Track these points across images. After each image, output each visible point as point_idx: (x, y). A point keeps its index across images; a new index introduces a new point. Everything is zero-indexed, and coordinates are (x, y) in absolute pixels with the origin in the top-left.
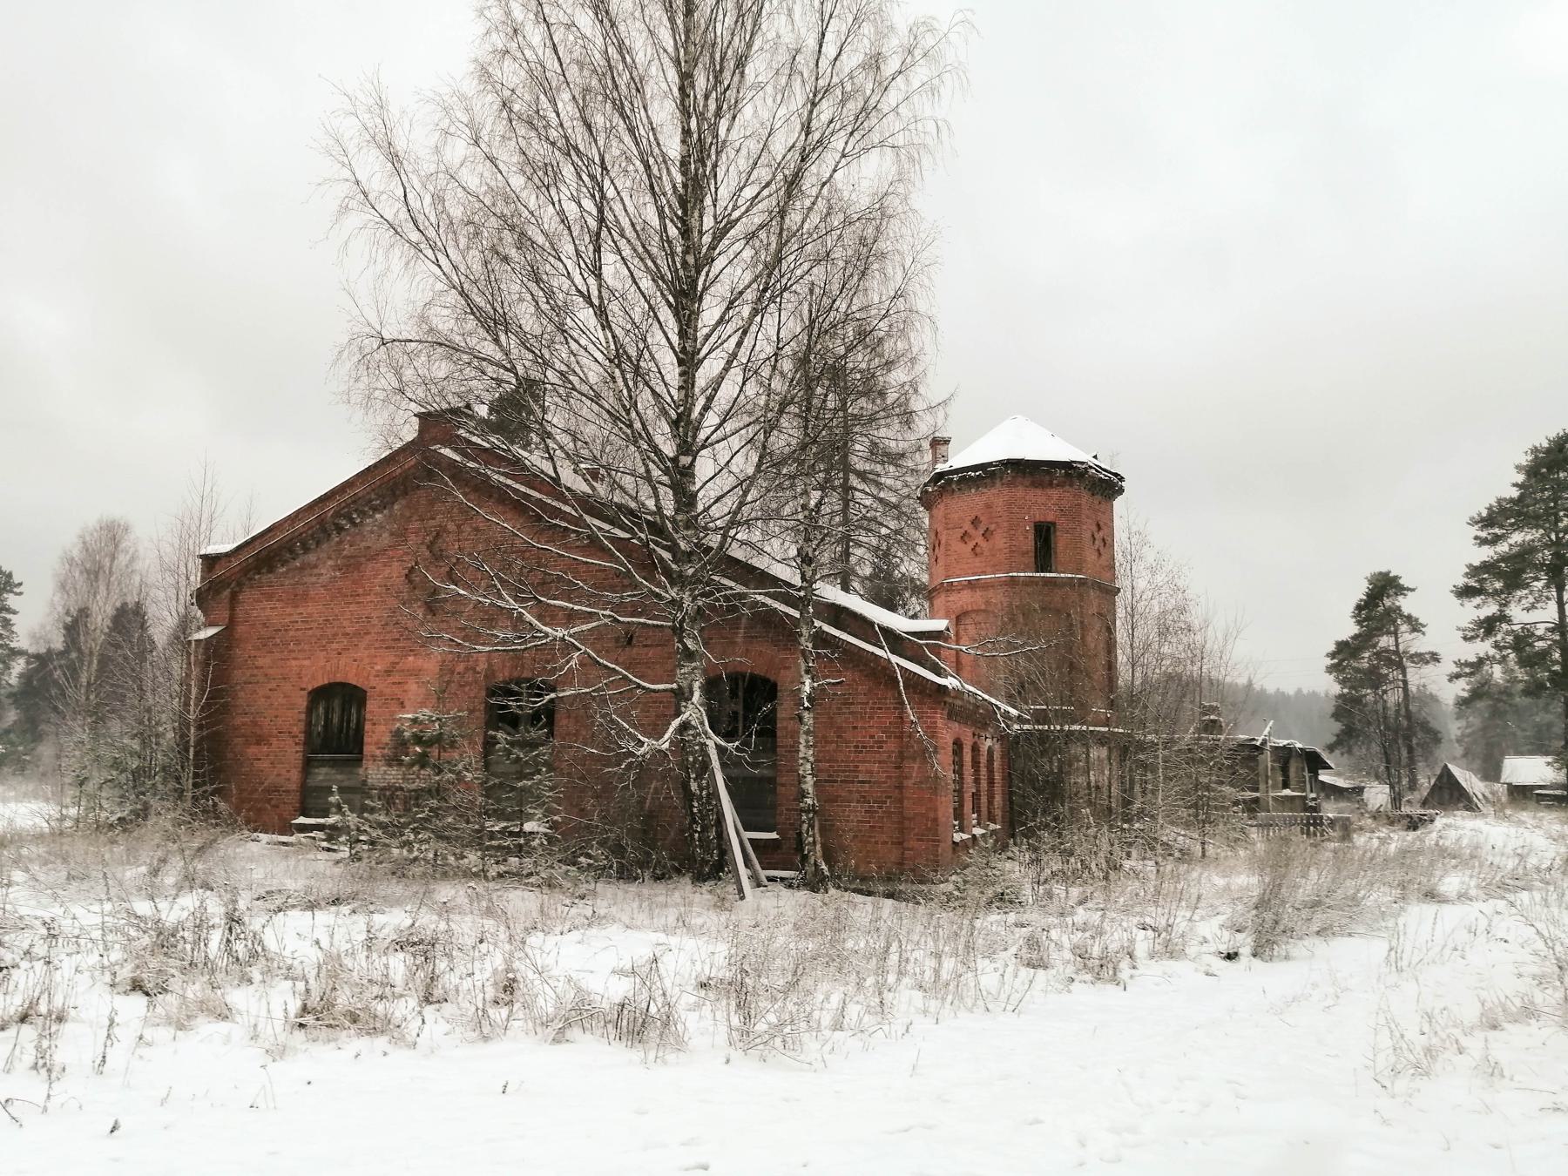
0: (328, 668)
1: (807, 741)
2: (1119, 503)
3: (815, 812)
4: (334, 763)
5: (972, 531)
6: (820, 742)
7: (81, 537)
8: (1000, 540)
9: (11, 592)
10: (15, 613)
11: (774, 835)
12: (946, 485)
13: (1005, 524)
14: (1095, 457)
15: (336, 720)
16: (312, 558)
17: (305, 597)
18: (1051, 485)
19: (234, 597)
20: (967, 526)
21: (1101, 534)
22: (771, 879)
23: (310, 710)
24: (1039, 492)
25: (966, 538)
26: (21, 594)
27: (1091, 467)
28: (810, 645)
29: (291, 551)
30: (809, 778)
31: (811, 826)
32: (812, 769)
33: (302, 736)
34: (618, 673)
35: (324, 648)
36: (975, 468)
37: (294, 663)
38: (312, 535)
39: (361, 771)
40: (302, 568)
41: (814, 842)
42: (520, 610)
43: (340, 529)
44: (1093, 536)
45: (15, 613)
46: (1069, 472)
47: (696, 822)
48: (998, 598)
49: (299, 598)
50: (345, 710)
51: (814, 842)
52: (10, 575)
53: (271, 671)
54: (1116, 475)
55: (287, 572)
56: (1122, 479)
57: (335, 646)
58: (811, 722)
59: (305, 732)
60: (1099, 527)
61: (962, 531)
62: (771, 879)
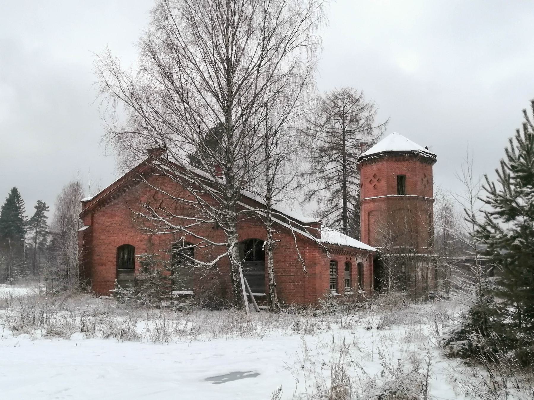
0: (123, 239)
1: (271, 262)
2: (435, 166)
3: (275, 286)
4: (126, 272)
5: (373, 179)
6: (276, 262)
7: (64, 190)
8: (383, 183)
9: (45, 210)
10: (47, 218)
11: (264, 294)
12: (364, 162)
13: (386, 176)
14: (426, 148)
15: (126, 256)
16: (116, 201)
17: (115, 216)
18: (404, 160)
19: (93, 216)
20: (372, 178)
21: (426, 178)
22: (261, 309)
23: (118, 254)
24: (399, 163)
25: (371, 182)
26: (48, 211)
27: (420, 153)
28: (270, 229)
29: (110, 199)
30: (272, 274)
31: (273, 291)
32: (273, 271)
33: (115, 263)
34: (204, 240)
35: (121, 233)
36: (373, 155)
37: (112, 238)
38: (116, 194)
39: (134, 274)
40: (114, 205)
41: (274, 296)
42: (164, 220)
43: (124, 191)
44: (422, 179)
45: (47, 218)
46: (412, 155)
47: (236, 290)
48: (384, 206)
49: (112, 216)
50: (129, 254)
51: (274, 296)
52: (45, 204)
53: (105, 241)
54: (433, 155)
55: (109, 206)
56: (436, 156)
57: (124, 231)
58: (272, 255)
59: (117, 261)
60: (425, 176)
61: (370, 179)
62: (261, 309)
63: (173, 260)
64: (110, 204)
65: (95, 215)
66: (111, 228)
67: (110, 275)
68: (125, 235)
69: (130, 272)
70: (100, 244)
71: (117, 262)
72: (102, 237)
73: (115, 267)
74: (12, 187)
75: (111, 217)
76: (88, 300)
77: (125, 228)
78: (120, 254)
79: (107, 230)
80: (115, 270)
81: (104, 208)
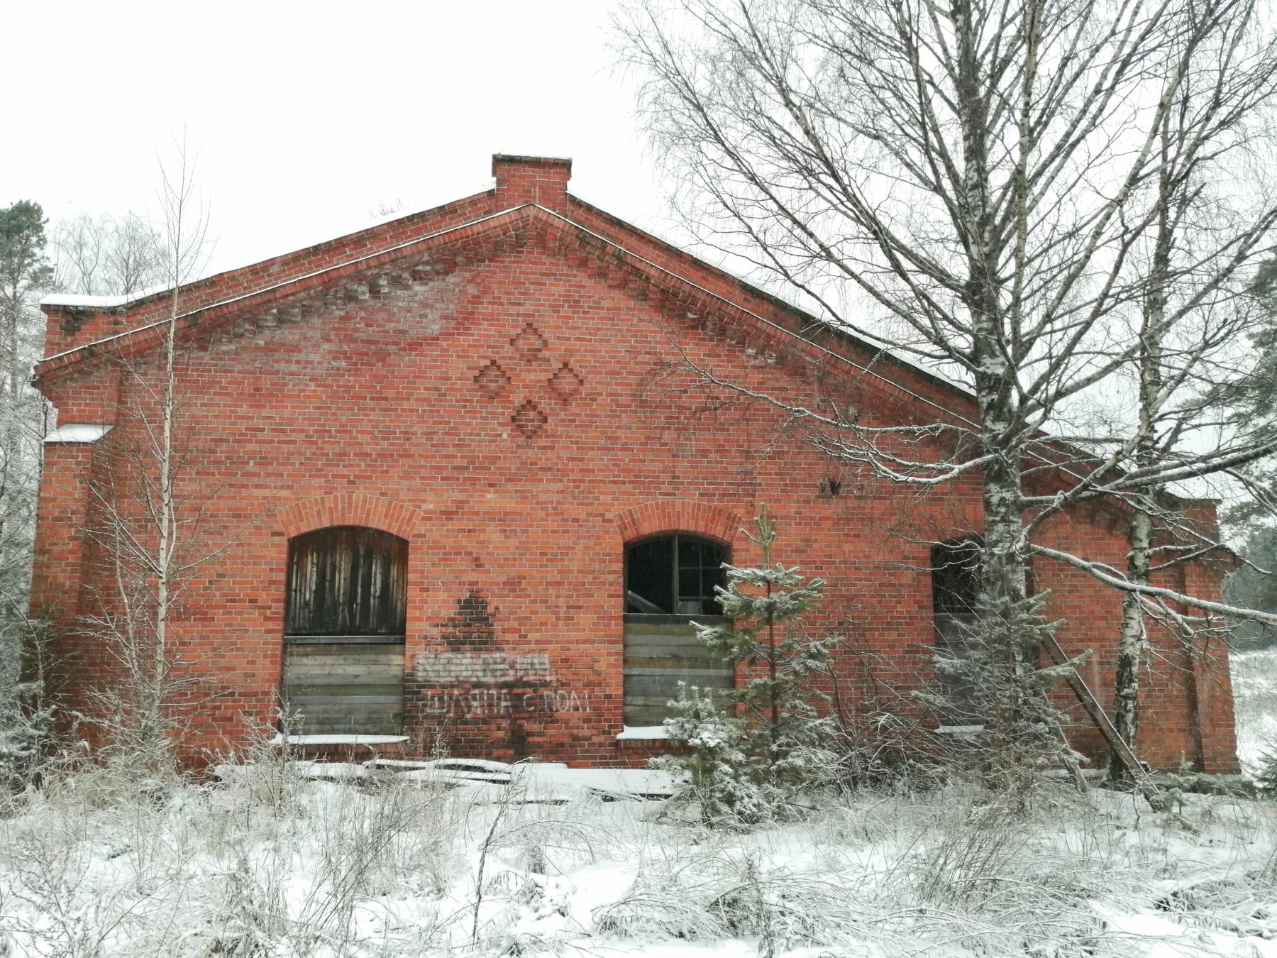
16: (289, 335)
29: (254, 322)
33: (279, 608)
40: (269, 349)
63: (1014, 484)
66: (250, 447)
74: (32, 198)
75: (257, 396)
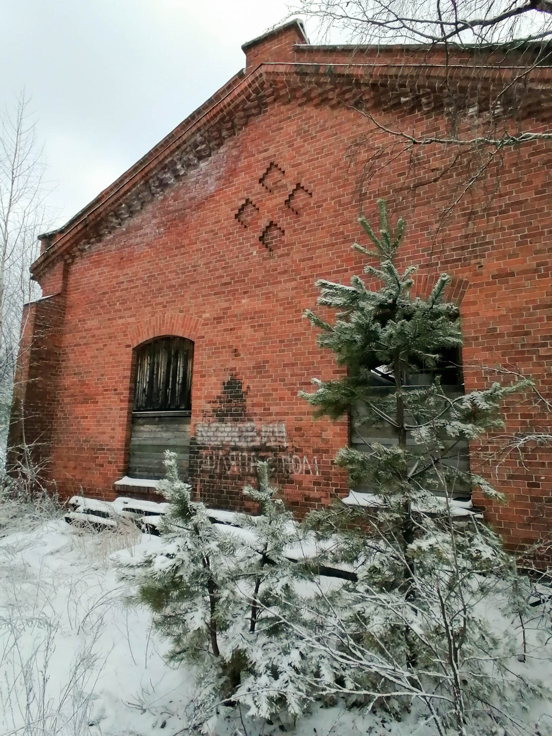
0: (153, 323)
15: (162, 371)
16: (136, 220)
19: (66, 273)
23: (136, 367)
33: (126, 393)
37: (120, 321)
40: (128, 232)
43: (163, 185)
55: (114, 239)
64: (118, 232)
65: (73, 268)
66: (117, 294)
67: (108, 430)
68: (160, 308)
69: (174, 419)
70: (85, 341)
71: (133, 390)
72: (90, 324)
73: (125, 405)
76: (447, 560)
77: (161, 289)
78: (142, 366)
79: (105, 303)
80: (125, 413)
81: (100, 245)
